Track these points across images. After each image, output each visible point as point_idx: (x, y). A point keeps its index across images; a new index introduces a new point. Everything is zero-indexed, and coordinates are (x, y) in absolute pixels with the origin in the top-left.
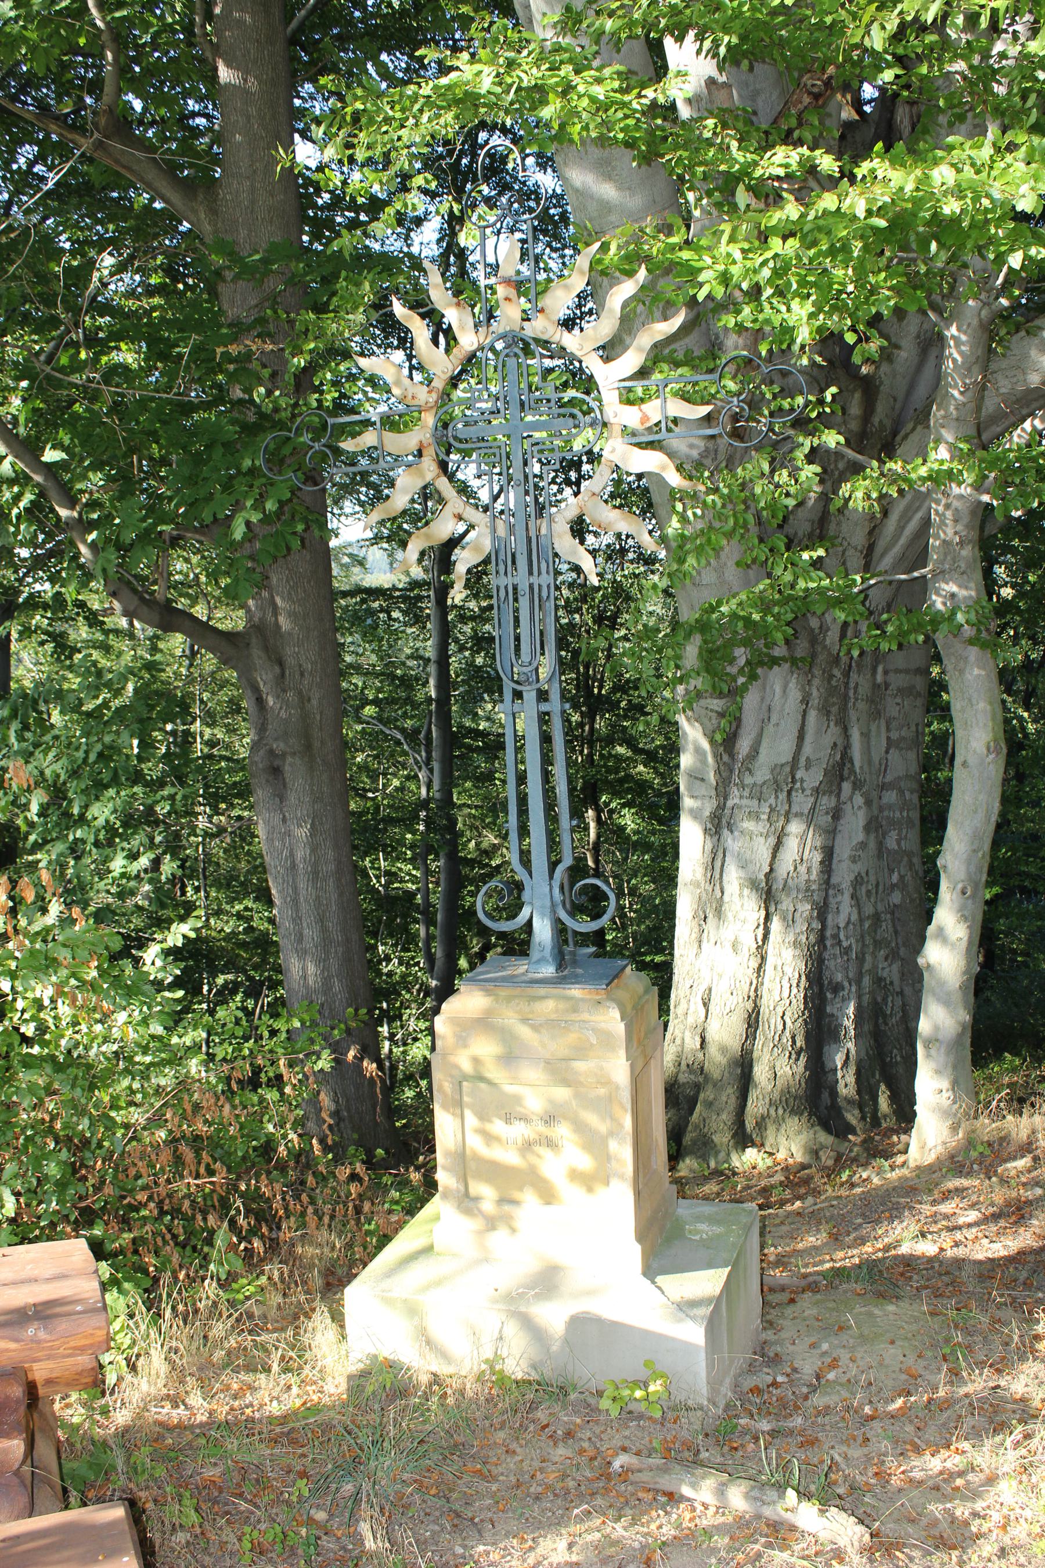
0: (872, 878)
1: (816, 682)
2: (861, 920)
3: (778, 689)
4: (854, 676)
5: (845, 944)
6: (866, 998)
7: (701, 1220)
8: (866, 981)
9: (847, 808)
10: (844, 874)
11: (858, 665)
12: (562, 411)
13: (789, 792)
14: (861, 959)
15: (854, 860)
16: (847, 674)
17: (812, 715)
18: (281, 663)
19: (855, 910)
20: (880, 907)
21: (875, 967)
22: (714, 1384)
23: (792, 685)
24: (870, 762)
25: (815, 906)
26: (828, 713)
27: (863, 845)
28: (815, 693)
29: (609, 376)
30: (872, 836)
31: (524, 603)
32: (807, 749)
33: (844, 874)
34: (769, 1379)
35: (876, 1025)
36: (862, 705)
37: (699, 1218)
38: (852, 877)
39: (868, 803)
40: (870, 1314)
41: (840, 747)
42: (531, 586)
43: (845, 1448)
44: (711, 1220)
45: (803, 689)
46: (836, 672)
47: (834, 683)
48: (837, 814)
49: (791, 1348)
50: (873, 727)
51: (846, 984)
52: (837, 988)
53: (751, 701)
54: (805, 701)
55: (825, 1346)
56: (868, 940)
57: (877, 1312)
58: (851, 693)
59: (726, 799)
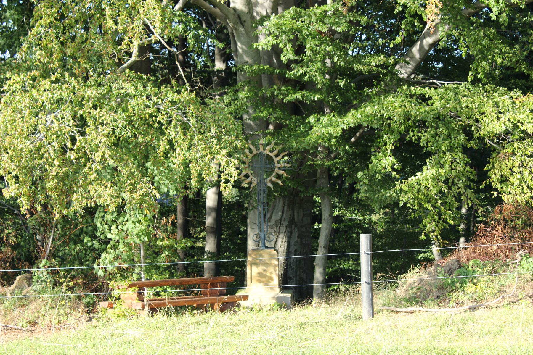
8: (298, 278)
9: (293, 231)
14: (296, 272)
15: (295, 245)
17: (286, 207)
23: (281, 200)
27: (297, 241)
28: (286, 202)
32: (284, 216)
39: (298, 230)
46: (292, 197)
54: (284, 203)
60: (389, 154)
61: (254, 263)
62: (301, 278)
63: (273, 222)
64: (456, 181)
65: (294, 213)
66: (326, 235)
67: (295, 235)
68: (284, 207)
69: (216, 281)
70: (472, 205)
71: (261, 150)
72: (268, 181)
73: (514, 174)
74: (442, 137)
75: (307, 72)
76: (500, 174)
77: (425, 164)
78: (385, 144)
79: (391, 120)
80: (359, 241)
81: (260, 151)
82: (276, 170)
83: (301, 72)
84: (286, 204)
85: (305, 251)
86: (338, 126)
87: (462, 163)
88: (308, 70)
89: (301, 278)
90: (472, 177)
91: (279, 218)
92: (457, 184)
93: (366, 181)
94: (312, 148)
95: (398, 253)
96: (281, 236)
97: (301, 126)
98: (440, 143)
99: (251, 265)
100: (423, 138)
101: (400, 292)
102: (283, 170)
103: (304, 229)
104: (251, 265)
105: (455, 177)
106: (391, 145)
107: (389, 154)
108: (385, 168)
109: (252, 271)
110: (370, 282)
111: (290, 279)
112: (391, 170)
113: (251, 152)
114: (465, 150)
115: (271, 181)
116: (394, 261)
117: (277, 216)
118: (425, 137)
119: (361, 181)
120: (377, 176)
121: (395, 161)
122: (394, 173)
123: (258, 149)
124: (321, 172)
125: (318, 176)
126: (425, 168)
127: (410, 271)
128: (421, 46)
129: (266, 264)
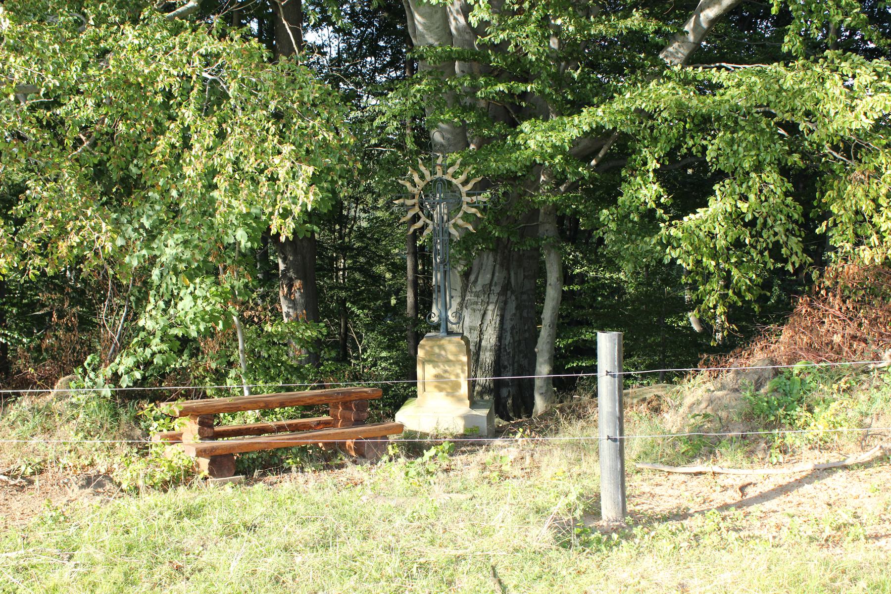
8: (516, 365)
14: (514, 357)
15: (511, 320)
17: (498, 266)
27: (515, 315)
32: (495, 279)
39: (517, 299)
54: (495, 261)
60: (651, 180)
61: (431, 360)
62: (520, 366)
63: (478, 288)
64: (770, 222)
65: (509, 274)
66: (553, 308)
67: (512, 306)
68: (495, 266)
69: (348, 399)
70: (801, 265)
71: (439, 174)
72: (451, 225)
73: (881, 209)
74: (744, 145)
75: (511, 38)
76: (854, 209)
77: (713, 193)
78: (645, 164)
79: (654, 120)
80: (596, 343)
81: (437, 176)
82: (465, 207)
83: (501, 36)
84: (498, 261)
85: (526, 327)
86: (564, 130)
87: (779, 191)
88: (514, 34)
89: (520, 366)
90: (796, 216)
91: (488, 282)
92: (772, 227)
93: (613, 226)
94: (521, 169)
95: (665, 348)
96: (491, 307)
97: (509, 137)
98: (741, 156)
99: (423, 363)
100: (710, 147)
101: (672, 421)
102: (476, 207)
103: (525, 297)
104: (423, 363)
105: (768, 215)
106: (655, 161)
107: (651, 180)
108: (645, 203)
109: (425, 373)
110: (618, 437)
111: (505, 367)
112: (654, 206)
113: (422, 177)
114: (784, 171)
115: (455, 226)
116: (651, 336)
117: (484, 278)
118: (714, 148)
119: (604, 225)
120: (632, 216)
121: (661, 190)
122: (660, 212)
123: (433, 173)
124: (545, 213)
125: (540, 219)
126: (711, 200)
127: (689, 380)
128: (697, 23)
129: (448, 361)
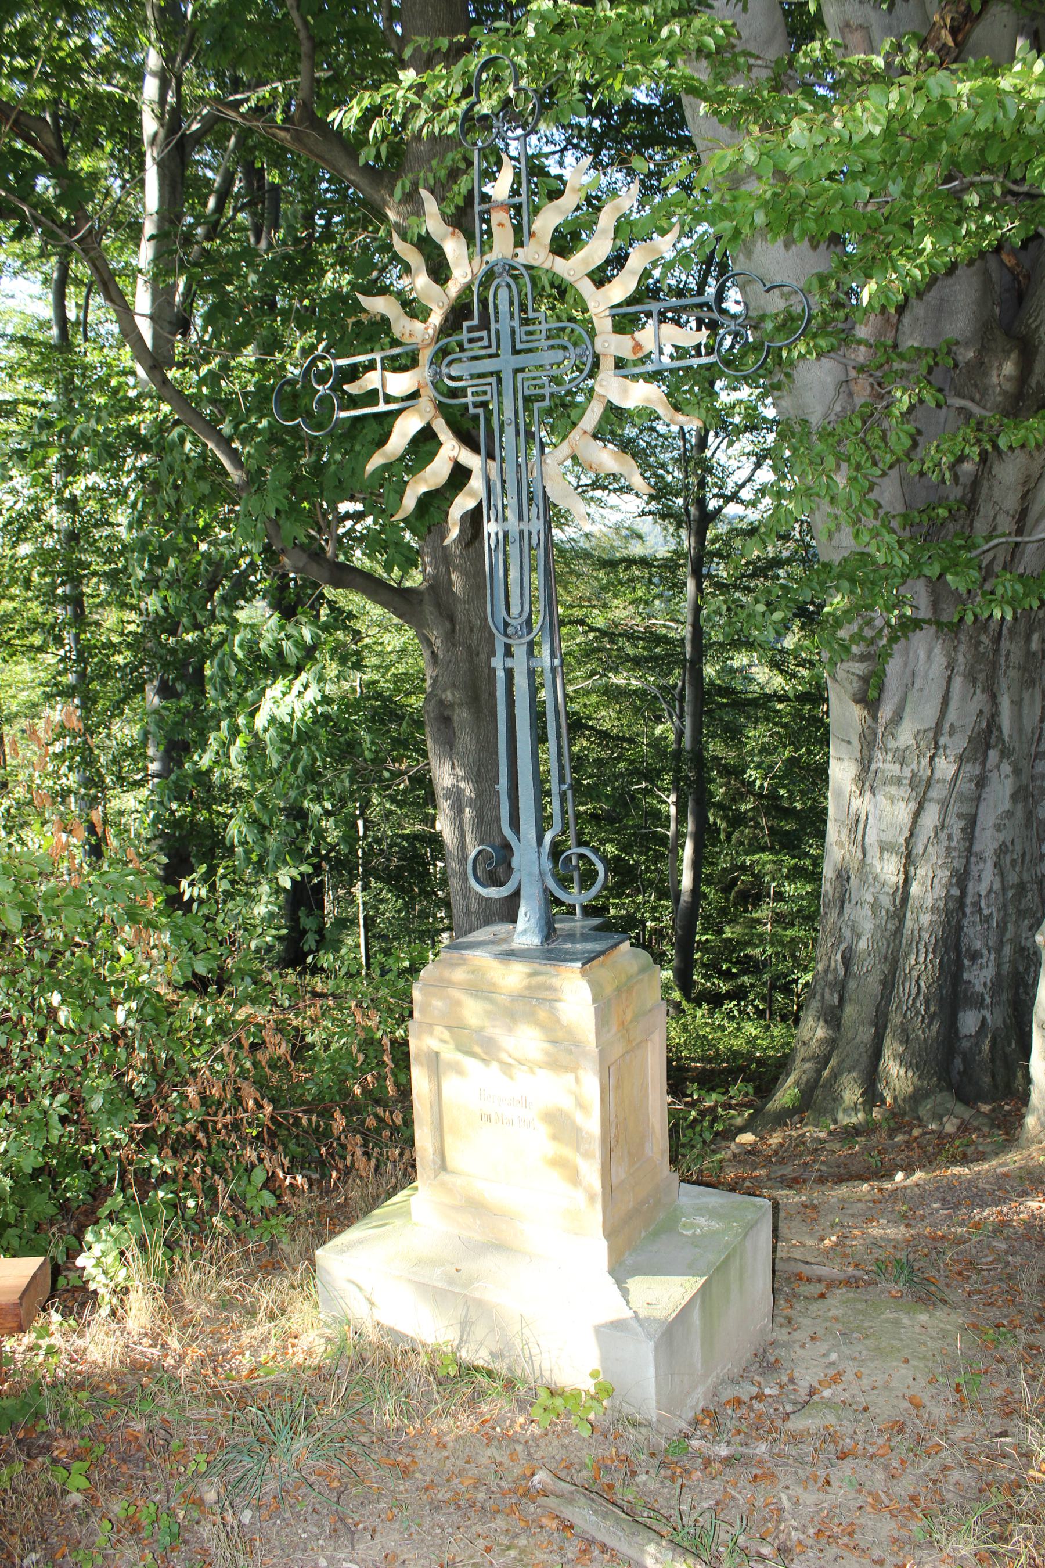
0: (1018, 848)
1: (963, 648)
2: (1004, 889)
3: (922, 654)
4: (1005, 644)
5: (986, 912)
6: (1006, 968)
7: (703, 1211)
8: (1007, 950)
9: (994, 776)
10: (987, 842)
11: (1011, 631)
12: (551, 342)
13: (932, 758)
14: (1002, 928)
15: (998, 828)
16: (998, 639)
17: (958, 682)
18: (452, 619)
19: (998, 879)
20: (1026, 877)
21: (1017, 936)
22: (669, 1401)
23: (937, 650)
24: (1021, 730)
25: (954, 873)
26: (975, 680)
27: (1009, 814)
28: (961, 659)
29: (602, 303)
30: (1020, 806)
31: (513, 550)
32: (952, 716)
33: (987, 842)
34: (755, 1390)
35: (1017, 993)
36: (1013, 673)
37: (700, 1211)
38: (996, 846)
39: (1017, 772)
40: (897, 1323)
41: (987, 714)
42: (521, 533)
43: (799, 1490)
44: (713, 1213)
45: (948, 655)
46: (984, 638)
47: (982, 649)
48: (981, 782)
49: (800, 1352)
50: (1026, 696)
51: (985, 952)
52: (975, 956)
53: (893, 667)
54: (951, 667)
55: (834, 1356)
56: (1011, 910)
57: (906, 1321)
58: (1002, 660)
59: (870, 761)
